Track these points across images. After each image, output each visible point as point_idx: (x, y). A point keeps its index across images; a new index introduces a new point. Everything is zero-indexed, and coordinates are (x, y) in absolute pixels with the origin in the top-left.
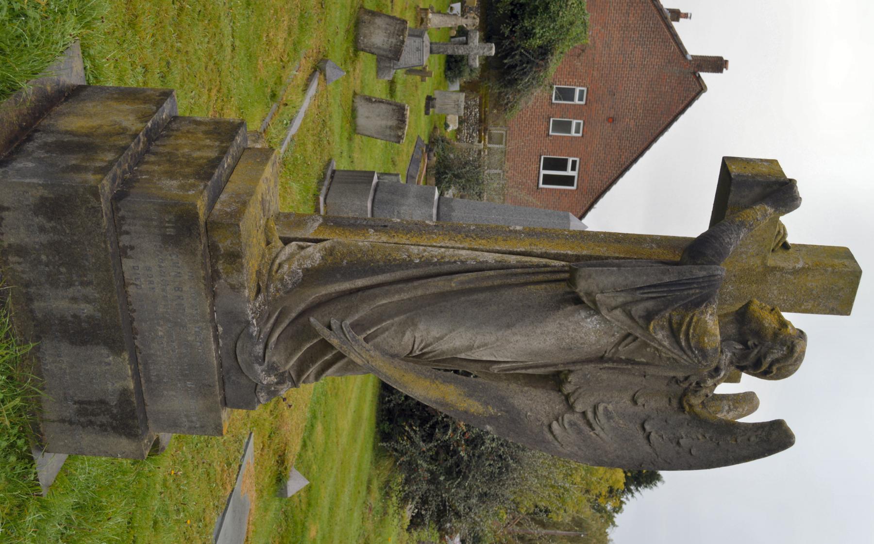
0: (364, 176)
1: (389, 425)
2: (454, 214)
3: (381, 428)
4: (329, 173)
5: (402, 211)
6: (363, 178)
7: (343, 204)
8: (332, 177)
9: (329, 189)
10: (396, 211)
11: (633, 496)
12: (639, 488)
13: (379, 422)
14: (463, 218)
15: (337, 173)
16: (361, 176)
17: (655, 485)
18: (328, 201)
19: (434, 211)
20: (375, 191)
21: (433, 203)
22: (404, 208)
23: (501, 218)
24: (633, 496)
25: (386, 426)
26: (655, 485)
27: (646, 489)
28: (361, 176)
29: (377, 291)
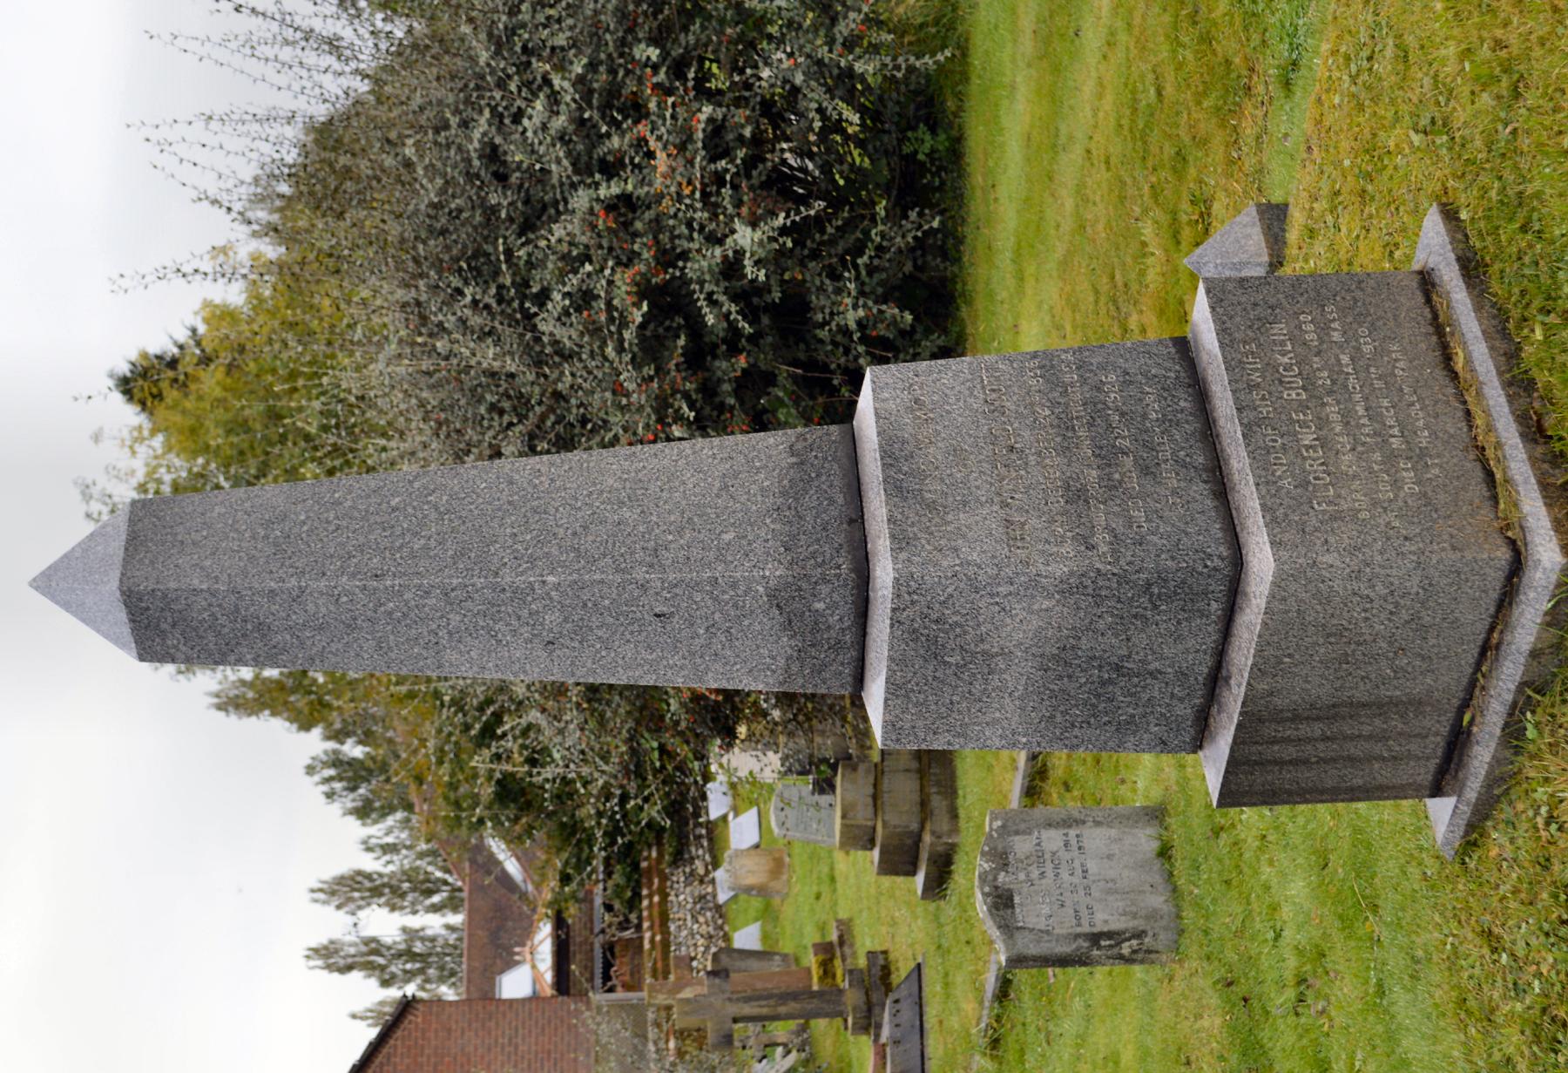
0: (1280, 763)
1: (916, 152)
2: (775, 571)
3: (942, 137)
4: (1482, 756)
5: (1068, 549)
6: (1291, 752)
7: (1409, 547)
8: (1458, 742)
9: (1489, 649)
10: (1104, 548)
11: (194, 331)
12: (175, 350)
13: (955, 154)
14: (720, 558)
15: (1425, 773)
16: (1295, 762)
17: (133, 364)
18: (1503, 555)
19: (884, 573)
20: (1216, 678)
21: (895, 622)
22: (1060, 570)
23: (507, 578)
24: (194, 331)
25: (925, 143)
26: (133, 364)
27: (158, 351)
28: (1295, 762)
29: (763, 821)
